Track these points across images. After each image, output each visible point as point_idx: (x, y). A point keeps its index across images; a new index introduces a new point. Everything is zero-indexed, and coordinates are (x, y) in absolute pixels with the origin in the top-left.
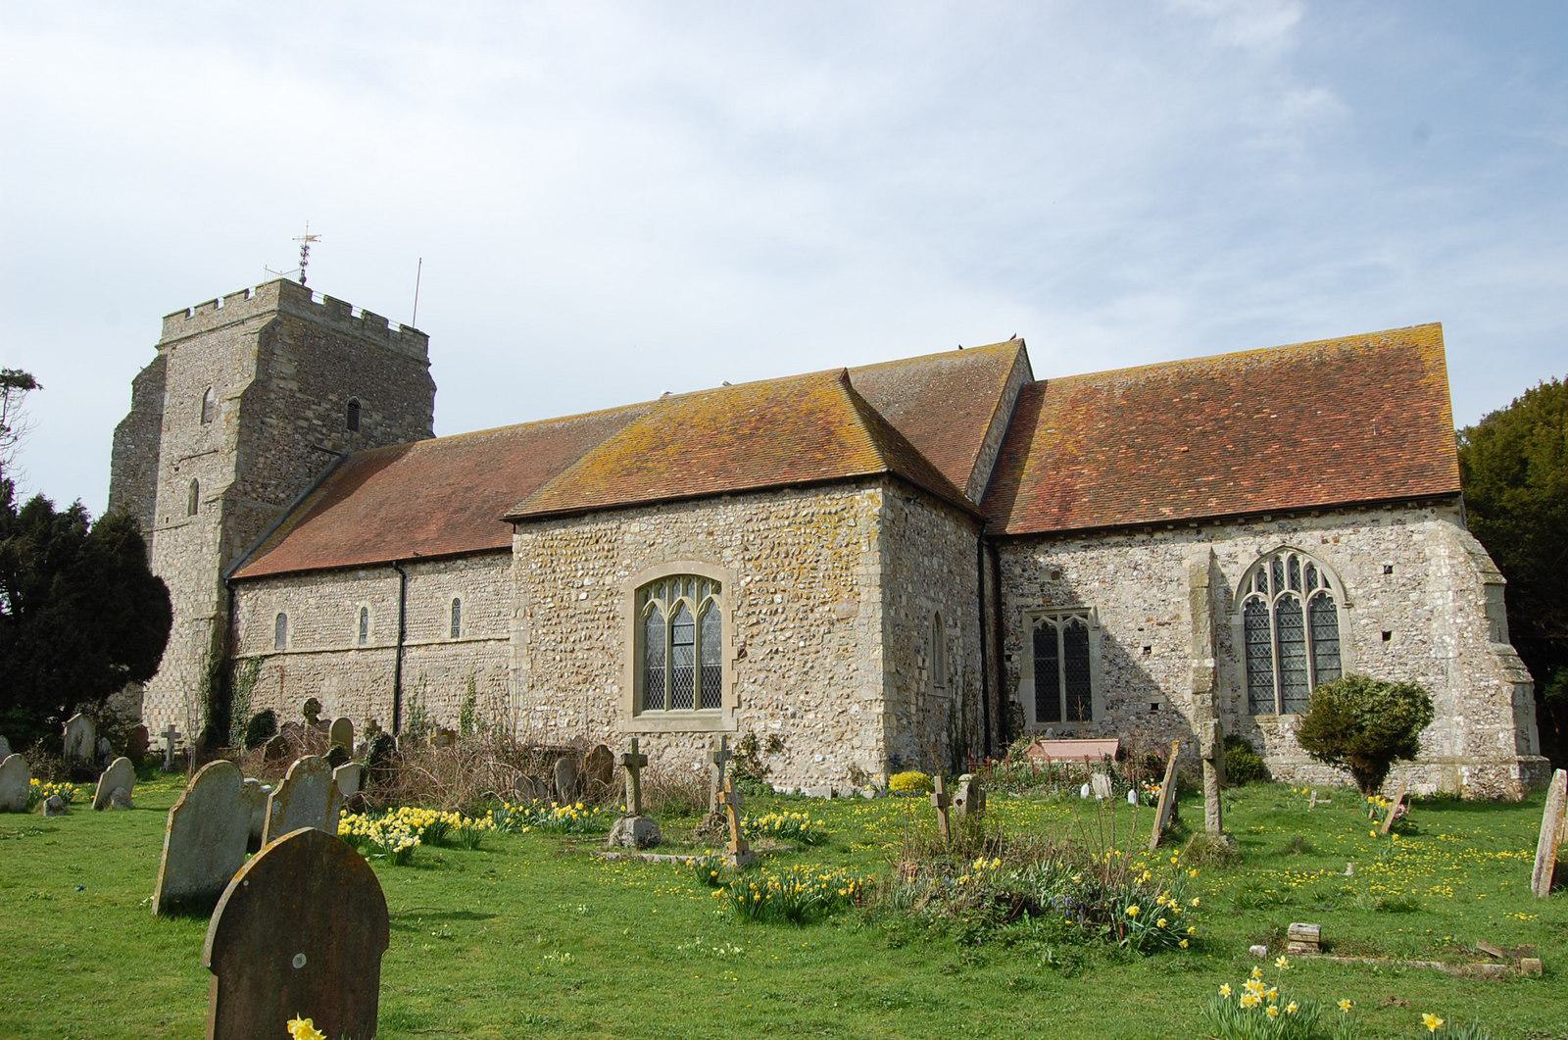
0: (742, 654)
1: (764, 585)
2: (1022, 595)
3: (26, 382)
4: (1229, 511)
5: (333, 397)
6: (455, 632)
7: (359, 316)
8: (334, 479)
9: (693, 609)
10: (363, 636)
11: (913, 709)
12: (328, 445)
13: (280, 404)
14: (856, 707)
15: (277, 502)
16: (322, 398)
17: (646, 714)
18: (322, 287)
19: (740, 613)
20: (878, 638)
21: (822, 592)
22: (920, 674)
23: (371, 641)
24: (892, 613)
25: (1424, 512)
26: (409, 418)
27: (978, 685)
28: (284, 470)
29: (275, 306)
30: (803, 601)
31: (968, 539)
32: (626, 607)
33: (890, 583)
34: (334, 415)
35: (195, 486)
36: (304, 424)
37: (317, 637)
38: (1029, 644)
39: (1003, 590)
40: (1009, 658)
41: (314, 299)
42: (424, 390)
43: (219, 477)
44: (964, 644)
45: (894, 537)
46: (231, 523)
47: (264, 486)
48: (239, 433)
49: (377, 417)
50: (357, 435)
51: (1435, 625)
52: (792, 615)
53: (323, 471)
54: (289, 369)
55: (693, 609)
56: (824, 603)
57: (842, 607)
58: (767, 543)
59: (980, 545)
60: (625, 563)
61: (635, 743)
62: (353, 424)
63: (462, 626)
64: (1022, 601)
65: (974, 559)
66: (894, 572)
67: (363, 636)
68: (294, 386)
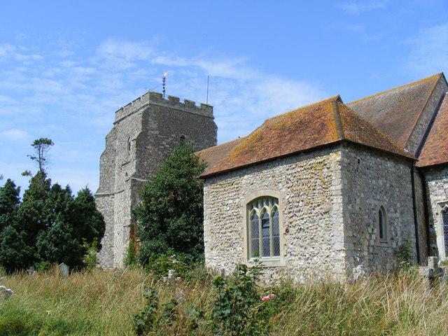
0: (287, 231)
1: (294, 199)
2: (436, 195)
3: (49, 142)
7: (183, 102)
9: (269, 209)
11: (366, 253)
13: (152, 140)
14: (333, 254)
16: (168, 136)
21: (318, 200)
22: (370, 236)
24: (350, 207)
26: (206, 141)
30: (310, 205)
42: (213, 128)
55: (269, 209)
56: (319, 205)
57: (325, 207)
59: (412, 173)
60: (243, 192)
65: (409, 179)
66: (351, 189)
68: (157, 132)
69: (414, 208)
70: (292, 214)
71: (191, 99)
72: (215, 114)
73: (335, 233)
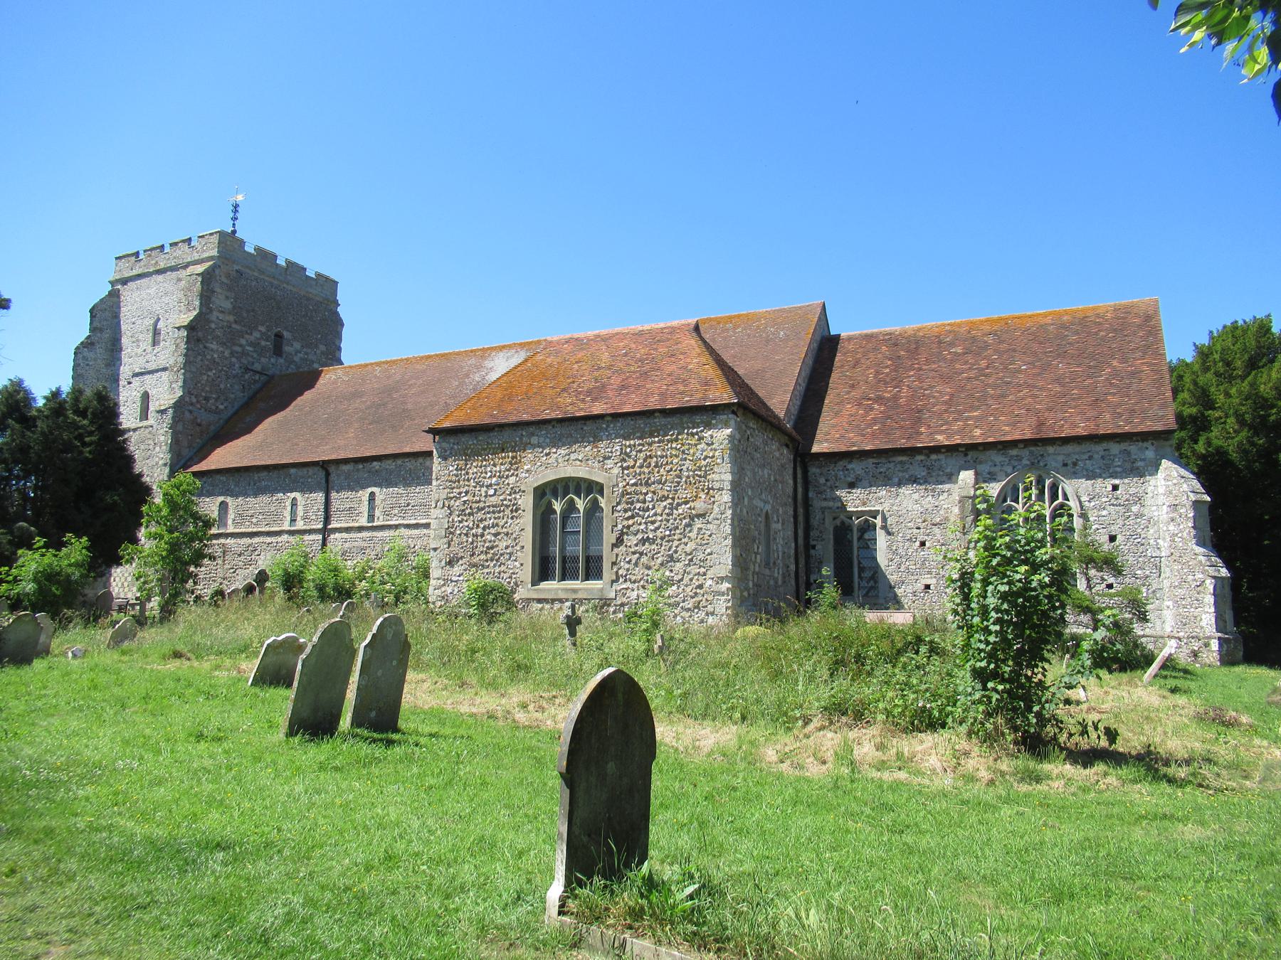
0: (619, 542)
4: (990, 440)
5: (263, 329)
6: (371, 517)
8: (273, 391)
9: (580, 504)
10: (293, 521)
11: (751, 584)
12: (257, 367)
15: (217, 411)
17: (544, 585)
18: (253, 238)
19: (619, 508)
20: (728, 530)
21: (683, 494)
23: (300, 525)
25: (1145, 444)
26: (322, 348)
27: (793, 567)
28: (222, 386)
29: (215, 253)
30: (670, 501)
31: (786, 455)
32: (526, 502)
33: (737, 488)
34: (263, 343)
35: (146, 397)
36: (238, 349)
37: (254, 520)
38: (830, 537)
39: (810, 495)
40: (814, 547)
41: (247, 249)
42: (335, 325)
43: (166, 391)
44: (783, 533)
45: (740, 453)
46: (180, 427)
47: (207, 399)
48: (186, 355)
49: (297, 345)
50: (281, 361)
51: (1152, 531)
52: (659, 511)
53: (255, 387)
54: (227, 305)
56: (686, 503)
58: (642, 455)
61: (573, 607)
62: (278, 351)
63: (377, 513)
64: (825, 504)
65: (791, 471)
67: (293, 521)
68: (231, 318)
69: (795, 517)
70: (630, 514)
71: (268, 247)
72: (340, 297)
73: (715, 548)
